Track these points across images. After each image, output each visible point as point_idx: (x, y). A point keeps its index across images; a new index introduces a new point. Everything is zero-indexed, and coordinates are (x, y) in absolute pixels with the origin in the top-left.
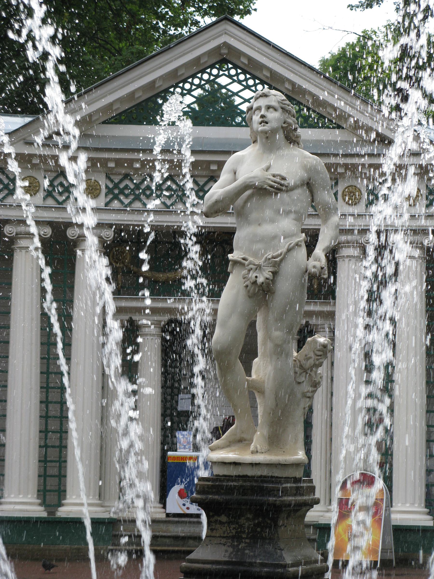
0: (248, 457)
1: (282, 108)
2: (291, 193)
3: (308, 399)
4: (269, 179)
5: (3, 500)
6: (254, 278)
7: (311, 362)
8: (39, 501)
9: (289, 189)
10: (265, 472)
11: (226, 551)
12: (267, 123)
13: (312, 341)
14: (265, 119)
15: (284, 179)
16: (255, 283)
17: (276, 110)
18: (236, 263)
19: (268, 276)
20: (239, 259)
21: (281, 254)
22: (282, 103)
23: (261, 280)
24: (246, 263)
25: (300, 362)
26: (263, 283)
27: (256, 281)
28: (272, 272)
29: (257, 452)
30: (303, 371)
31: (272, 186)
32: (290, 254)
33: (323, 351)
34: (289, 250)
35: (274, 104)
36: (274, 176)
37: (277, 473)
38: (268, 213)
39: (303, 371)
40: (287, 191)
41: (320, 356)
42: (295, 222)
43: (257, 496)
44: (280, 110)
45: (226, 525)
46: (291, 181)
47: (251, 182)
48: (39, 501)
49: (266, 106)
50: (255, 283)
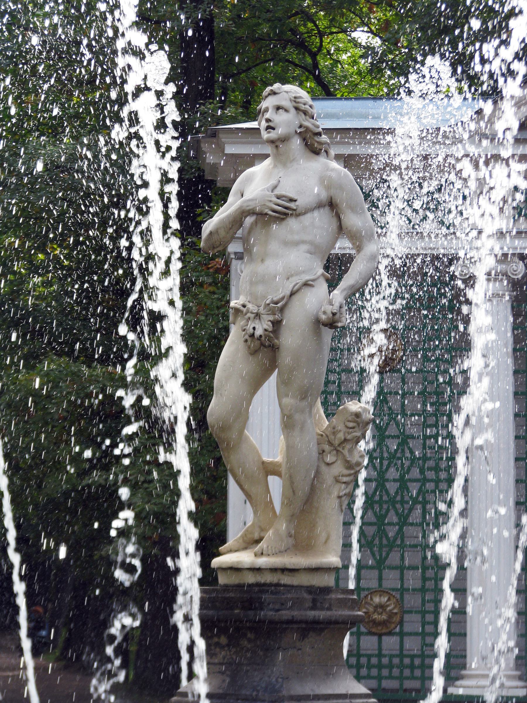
0: (263, 561)
1: (297, 109)
2: (302, 218)
3: (343, 486)
4: (271, 201)
5: (463, 672)
6: (251, 331)
7: (341, 436)
8: (518, 673)
9: (297, 214)
10: (268, 578)
11: (224, 681)
12: (273, 129)
13: (342, 409)
14: (271, 124)
15: (292, 200)
16: (252, 336)
17: (286, 111)
18: (237, 311)
19: (266, 327)
20: (239, 307)
21: (283, 298)
22: (295, 101)
23: (259, 332)
24: (245, 310)
25: (327, 436)
26: (261, 336)
27: (254, 334)
28: (273, 322)
29: (262, 554)
30: (332, 448)
31: (274, 211)
32: (295, 298)
33: (354, 422)
34: (292, 294)
35: (286, 103)
36: (278, 197)
37: (286, 580)
38: (274, 246)
39: (332, 448)
40: (298, 215)
41: (353, 428)
42: (309, 255)
43: (319, 616)
44: (293, 111)
45: (226, 649)
46: (302, 202)
47: (248, 206)
48: (518, 673)
49: (274, 106)
50: (252, 336)
